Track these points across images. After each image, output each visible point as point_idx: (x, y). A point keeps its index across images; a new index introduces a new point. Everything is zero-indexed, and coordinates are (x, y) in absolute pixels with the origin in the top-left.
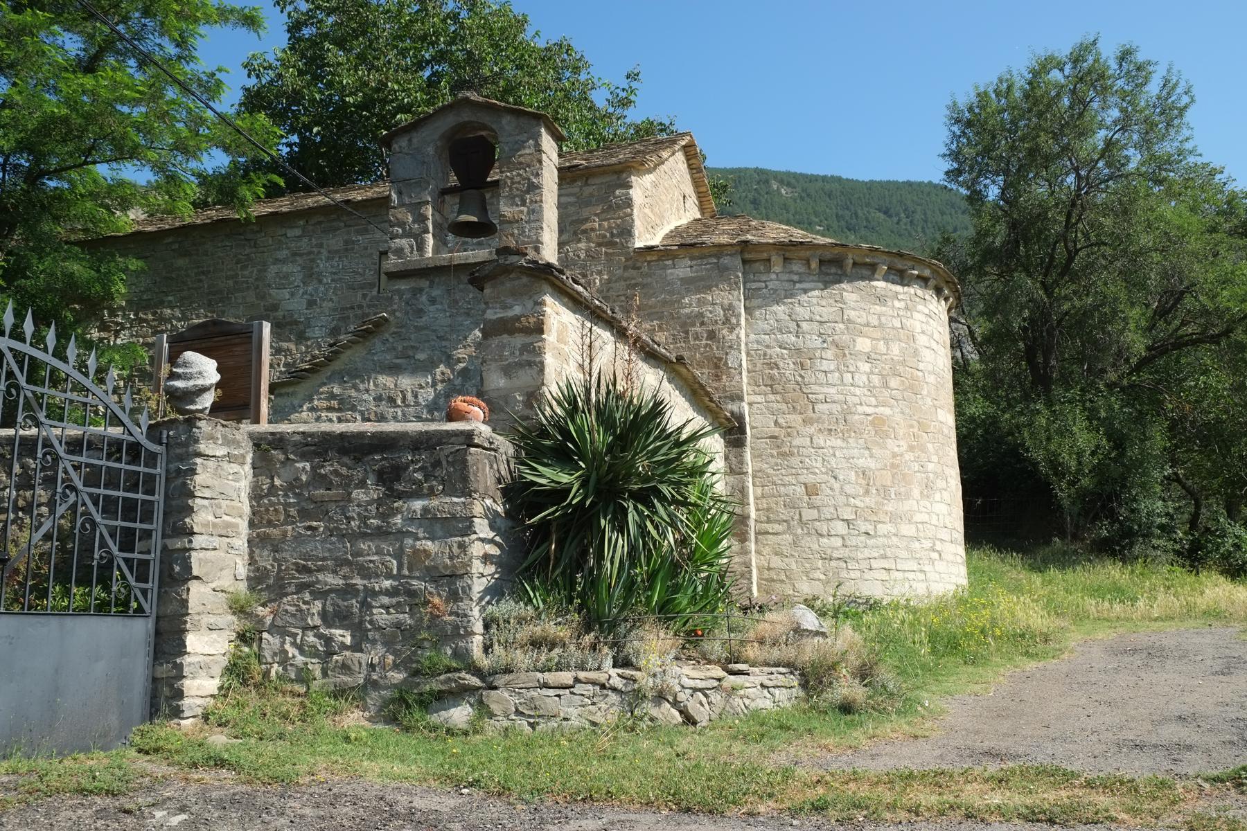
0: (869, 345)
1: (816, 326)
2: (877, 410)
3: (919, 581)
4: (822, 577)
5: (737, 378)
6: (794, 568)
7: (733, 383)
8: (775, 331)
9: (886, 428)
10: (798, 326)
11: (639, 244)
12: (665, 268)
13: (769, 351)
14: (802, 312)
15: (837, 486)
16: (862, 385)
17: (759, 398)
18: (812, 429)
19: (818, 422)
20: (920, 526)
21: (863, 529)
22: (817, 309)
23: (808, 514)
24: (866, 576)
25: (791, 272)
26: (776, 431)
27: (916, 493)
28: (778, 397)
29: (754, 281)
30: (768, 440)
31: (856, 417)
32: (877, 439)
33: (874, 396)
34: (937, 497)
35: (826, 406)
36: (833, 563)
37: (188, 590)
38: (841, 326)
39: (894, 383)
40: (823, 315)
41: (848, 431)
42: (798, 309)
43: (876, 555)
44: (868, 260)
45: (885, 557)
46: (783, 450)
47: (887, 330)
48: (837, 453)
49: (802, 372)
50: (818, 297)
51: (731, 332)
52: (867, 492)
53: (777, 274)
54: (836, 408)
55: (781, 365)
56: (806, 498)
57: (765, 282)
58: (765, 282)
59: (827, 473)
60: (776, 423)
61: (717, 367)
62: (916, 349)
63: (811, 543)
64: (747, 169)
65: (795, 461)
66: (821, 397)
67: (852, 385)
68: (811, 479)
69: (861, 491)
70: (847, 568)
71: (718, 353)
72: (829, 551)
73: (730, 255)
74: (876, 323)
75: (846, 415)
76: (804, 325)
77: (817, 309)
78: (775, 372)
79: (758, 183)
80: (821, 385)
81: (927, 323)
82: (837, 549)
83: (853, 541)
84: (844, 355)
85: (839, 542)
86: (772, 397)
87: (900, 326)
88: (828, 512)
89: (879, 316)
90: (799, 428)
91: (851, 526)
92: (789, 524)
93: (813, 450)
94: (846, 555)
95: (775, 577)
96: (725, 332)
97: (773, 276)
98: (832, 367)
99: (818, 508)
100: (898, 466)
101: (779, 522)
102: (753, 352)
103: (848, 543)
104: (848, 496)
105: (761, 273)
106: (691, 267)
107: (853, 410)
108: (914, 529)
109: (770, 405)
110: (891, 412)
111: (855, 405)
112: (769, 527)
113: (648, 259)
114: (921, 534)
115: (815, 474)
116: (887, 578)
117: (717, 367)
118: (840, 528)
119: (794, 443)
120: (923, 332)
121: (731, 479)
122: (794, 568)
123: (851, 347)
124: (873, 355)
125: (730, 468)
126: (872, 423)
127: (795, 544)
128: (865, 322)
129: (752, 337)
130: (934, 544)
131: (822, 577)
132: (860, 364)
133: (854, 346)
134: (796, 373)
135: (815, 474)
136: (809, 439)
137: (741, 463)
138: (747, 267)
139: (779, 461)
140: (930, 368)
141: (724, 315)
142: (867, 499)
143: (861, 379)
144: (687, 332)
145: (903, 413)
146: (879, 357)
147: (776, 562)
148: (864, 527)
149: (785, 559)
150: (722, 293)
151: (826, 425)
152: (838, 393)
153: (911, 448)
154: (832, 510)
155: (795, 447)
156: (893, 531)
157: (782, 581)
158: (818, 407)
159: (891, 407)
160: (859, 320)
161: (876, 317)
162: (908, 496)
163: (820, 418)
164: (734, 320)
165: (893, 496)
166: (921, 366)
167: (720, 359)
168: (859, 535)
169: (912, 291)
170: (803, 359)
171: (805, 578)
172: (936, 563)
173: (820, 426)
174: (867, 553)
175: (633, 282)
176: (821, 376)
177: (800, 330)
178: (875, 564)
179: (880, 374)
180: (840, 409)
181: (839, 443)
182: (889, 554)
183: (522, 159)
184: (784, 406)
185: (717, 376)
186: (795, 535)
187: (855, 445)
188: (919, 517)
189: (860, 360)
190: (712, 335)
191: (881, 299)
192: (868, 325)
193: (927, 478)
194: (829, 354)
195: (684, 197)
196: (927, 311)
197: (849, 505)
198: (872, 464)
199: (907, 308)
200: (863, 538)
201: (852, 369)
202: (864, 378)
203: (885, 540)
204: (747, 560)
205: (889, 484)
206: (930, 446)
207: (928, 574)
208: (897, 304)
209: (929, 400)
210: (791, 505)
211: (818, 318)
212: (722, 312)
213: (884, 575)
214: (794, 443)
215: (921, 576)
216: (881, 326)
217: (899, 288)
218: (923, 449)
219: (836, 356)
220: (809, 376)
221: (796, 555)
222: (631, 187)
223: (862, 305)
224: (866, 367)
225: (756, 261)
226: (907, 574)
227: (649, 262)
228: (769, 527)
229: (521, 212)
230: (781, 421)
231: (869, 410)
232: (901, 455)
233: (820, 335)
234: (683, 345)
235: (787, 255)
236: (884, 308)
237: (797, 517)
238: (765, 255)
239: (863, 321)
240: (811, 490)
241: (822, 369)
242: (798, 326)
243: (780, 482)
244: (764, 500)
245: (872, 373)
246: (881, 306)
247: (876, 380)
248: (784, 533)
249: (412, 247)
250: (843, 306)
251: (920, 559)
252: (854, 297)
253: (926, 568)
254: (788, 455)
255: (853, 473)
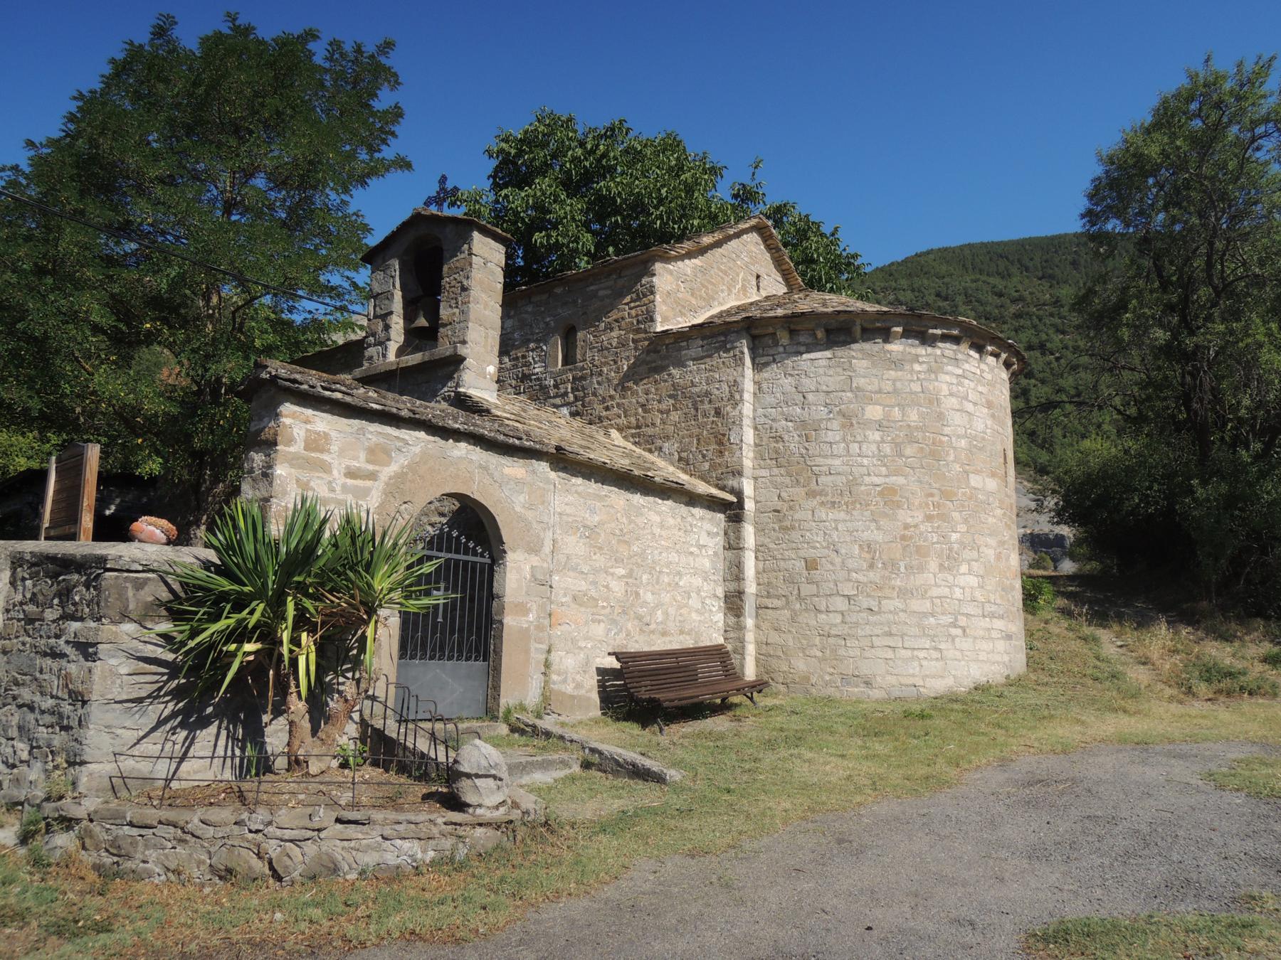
0: (881, 412)
1: (822, 396)
2: (887, 480)
3: (932, 659)
4: (819, 654)
5: (738, 453)
6: (791, 644)
7: (734, 459)
8: (782, 404)
9: (897, 498)
10: (804, 397)
11: (659, 329)
12: (680, 349)
13: (774, 425)
14: (808, 384)
15: (838, 560)
16: (870, 454)
17: (764, 473)
18: (814, 502)
19: (821, 495)
20: (937, 601)
21: (865, 605)
22: (823, 379)
23: (807, 589)
24: (867, 654)
25: (799, 344)
26: (779, 505)
27: (933, 565)
28: (783, 471)
29: (763, 356)
30: (770, 515)
31: (863, 488)
32: (887, 510)
33: (885, 465)
34: (964, 568)
35: (830, 478)
36: (831, 640)
37: (363, 639)
38: (849, 394)
39: (909, 451)
40: (830, 384)
41: (855, 502)
42: (805, 381)
43: (879, 632)
44: (878, 325)
45: (890, 634)
46: (784, 524)
47: (904, 396)
48: (840, 527)
49: (806, 444)
50: (825, 367)
51: (734, 408)
52: (871, 566)
53: (785, 347)
54: (841, 480)
55: (786, 438)
56: (805, 572)
57: (773, 355)
58: (773, 355)
59: (828, 548)
60: (779, 496)
61: (720, 443)
62: (941, 413)
63: (808, 619)
64: (1066, 234)
65: (795, 535)
66: (825, 469)
67: (859, 456)
68: (811, 553)
69: (865, 566)
70: (845, 645)
71: (722, 429)
72: (827, 628)
73: (737, 332)
74: (890, 389)
75: (852, 484)
76: (810, 397)
77: (823, 379)
78: (780, 445)
79: (1078, 245)
80: (826, 457)
81: (959, 384)
82: (835, 626)
83: (853, 618)
84: (852, 425)
85: (838, 619)
86: (776, 471)
87: (920, 390)
88: (827, 587)
89: (894, 381)
90: (801, 502)
91: (852, 602)
92: (787, 599)
93: (814, 524)
94: (845, 632)
95: (772, 653)
96: (729, 408)
97: (781, 349)
98: (838, 438)
99: (817, 583)
100: (911, 537)
101: (778, 597)
102: (759, 427)
103: (848, 619)
104: (849, 571)
105: (770, 347)
106: (702, 346)
107: (859, 481)
108: (928, 604)
109: (775, 478)
110: (905, 482)
111: (862, 476)
112: (769, 602)
113: (667, 342)
114: (939, 610)
115: (815, 548)
116: (892, 656)
117: (720, 443)
118: (841, 604)
119: (795, 517)
120: (951, 394)
121: (729, 554)
122: (791, 644)
123: (860, 415)
124: (885, 423)
125: (729, 543)
126: (881, 493)
127: (793, 620)
128: (877, 389)
129: (760, 411)
130: (956, 620)
131: (819, 654)
132: (869, 433)
133: (863, 415)
134: (801, 446)
135: (815, 548)
136: (810, 512)
137: (739, 538)
138: (757, 342)
139: (781, 535)
140: (961, 431)
141: (730, 392)
142: (871, 574)
143: (870, 449)
144: (697, 410)
145: (921, 482)
146: (893, 425)
147: (774, 637)
148: (866, 603)
149: (782, 635)
150: (728, 370)
151: (829, 498)
152: (844, 464)
153: (929, 518)
154: (831, 585)
155: (796, 521)
156: (901, 606)
157: (779, 657)
158: (822, 479)
159: (906, 476)
160: (870, 388)
161: (890, 383)
162: (921, 569)
163: (823, 490)
164: (738, 397)
165: (902, 569)
166: (947, 430)
167: (724, 435)
168: (860, 611)
169: (938, 352)
170: (808, 430)
171: (801, 655)
172: (957, 640)
173: (823, 498)
174: (869, 630)
175: (653, 365)
176: (825, 447)
177: (806, 402)
178: (877, 642)
179: (893, 442)
180: (845, 481)
181: (842, 515)
182: (894, 631)
183: (458, 265)
184: (787, 480)
185: (721, 452)
186: (793, 610)
187: (860, 517)
188: (935, 592)
189: (869, 429)
190: (718, 413)
191: (897, 364)
192: (880, 391)
193: (950, 549)
194: (835, 425)
195: (758, 277)
196: (960, 372)
197: (850, 580)
198: (879, 537)
199: (930, 370)
200: (864, 615)
201: (859, 439)
202: (874, 447)
203: (891, 616)
204: (741, 635)
205: (898, 556)
206: (956, 515)
207: (945, 653)
208: (917, 367)
209: (957, 468)
210: (790, 580)
211: (824, 388)
212: (727, 389)
213: (890, 654)
214: (795, 517)
215: (935, 654)
216: (896, 391)
217: (921, 350)
218: (944, 517)
219: (843, 426)
220: (813, 448)
221: (794, 630)
222: (654, 275)
223: (874, 371)
224: (877, 436)
225: (765, 335)
226: (916, 653)
227: (667, 345)
228: (769, 602)
229: (454, 314)
230: (784, 494)
231: (876, 480)
232: (916, 526)
233: (826, 405)
234: (693, 422)
235: (792, 327)
236: (900, 373)
237: (795, 592)
238: (771, 330)
239: (875, 387)
240: (811, 565)
241: (828, 440)
242: (804, 397)
243: (780, 556)
244: (765, 575)
245: (883, 441)
246: (896, 370)
247: (887, 449)
248: (782, 608)
249: (378, 353)
250: (850, 374)
251: (935, 636)
252: (865, 363)
253: (942, 646)
254: (789, 529)
255: (857, 547)
